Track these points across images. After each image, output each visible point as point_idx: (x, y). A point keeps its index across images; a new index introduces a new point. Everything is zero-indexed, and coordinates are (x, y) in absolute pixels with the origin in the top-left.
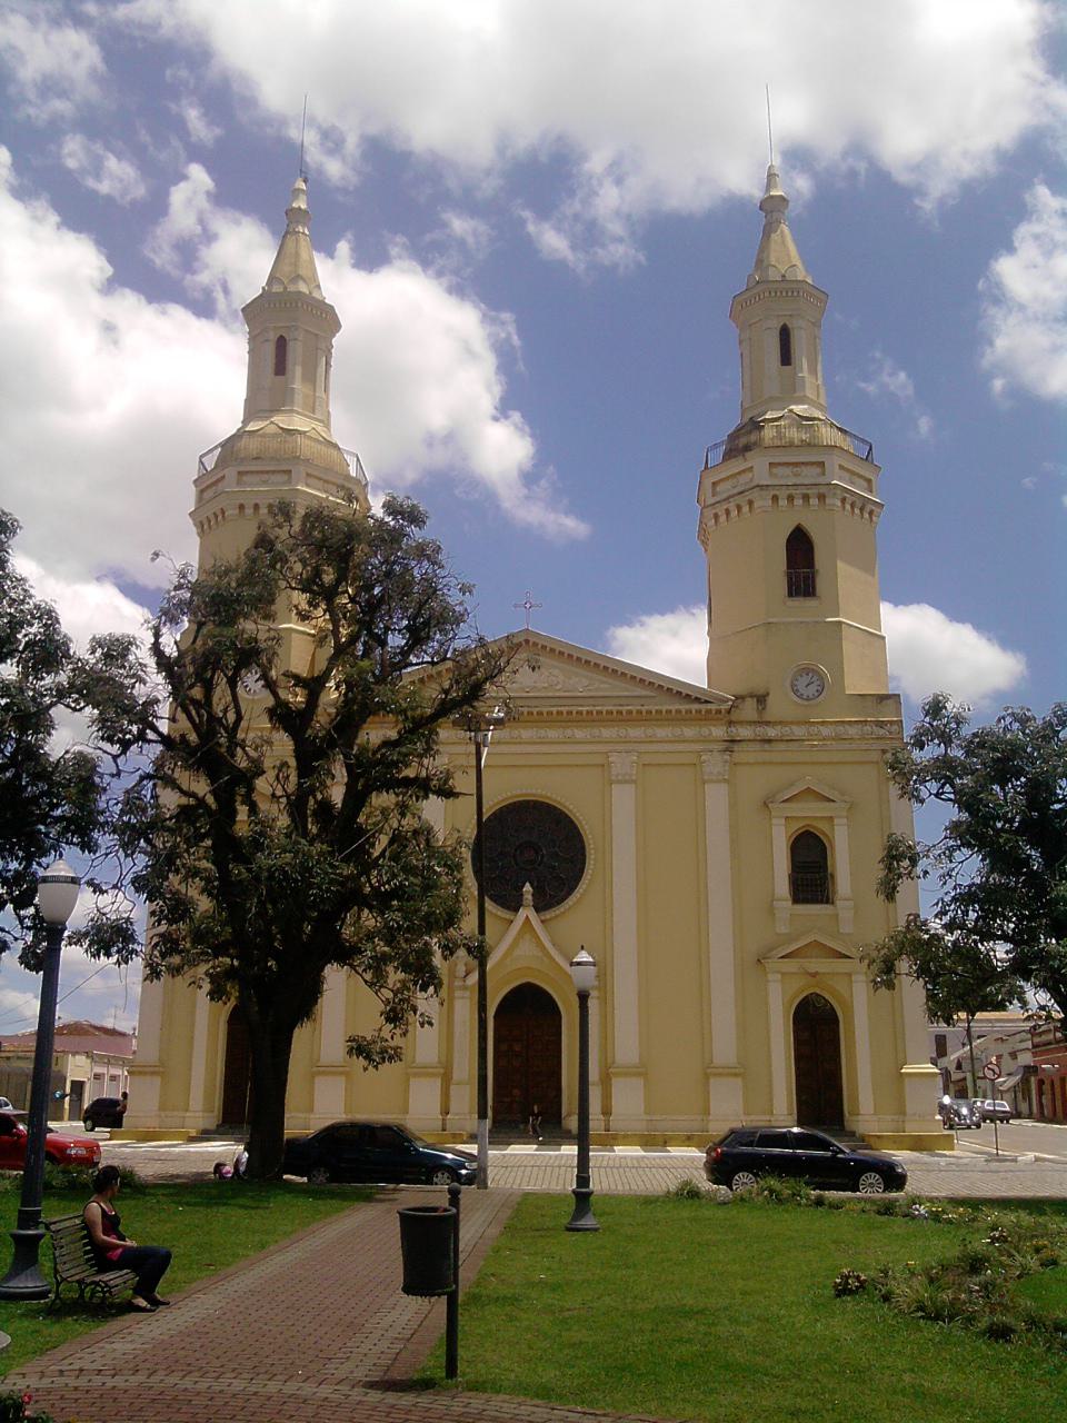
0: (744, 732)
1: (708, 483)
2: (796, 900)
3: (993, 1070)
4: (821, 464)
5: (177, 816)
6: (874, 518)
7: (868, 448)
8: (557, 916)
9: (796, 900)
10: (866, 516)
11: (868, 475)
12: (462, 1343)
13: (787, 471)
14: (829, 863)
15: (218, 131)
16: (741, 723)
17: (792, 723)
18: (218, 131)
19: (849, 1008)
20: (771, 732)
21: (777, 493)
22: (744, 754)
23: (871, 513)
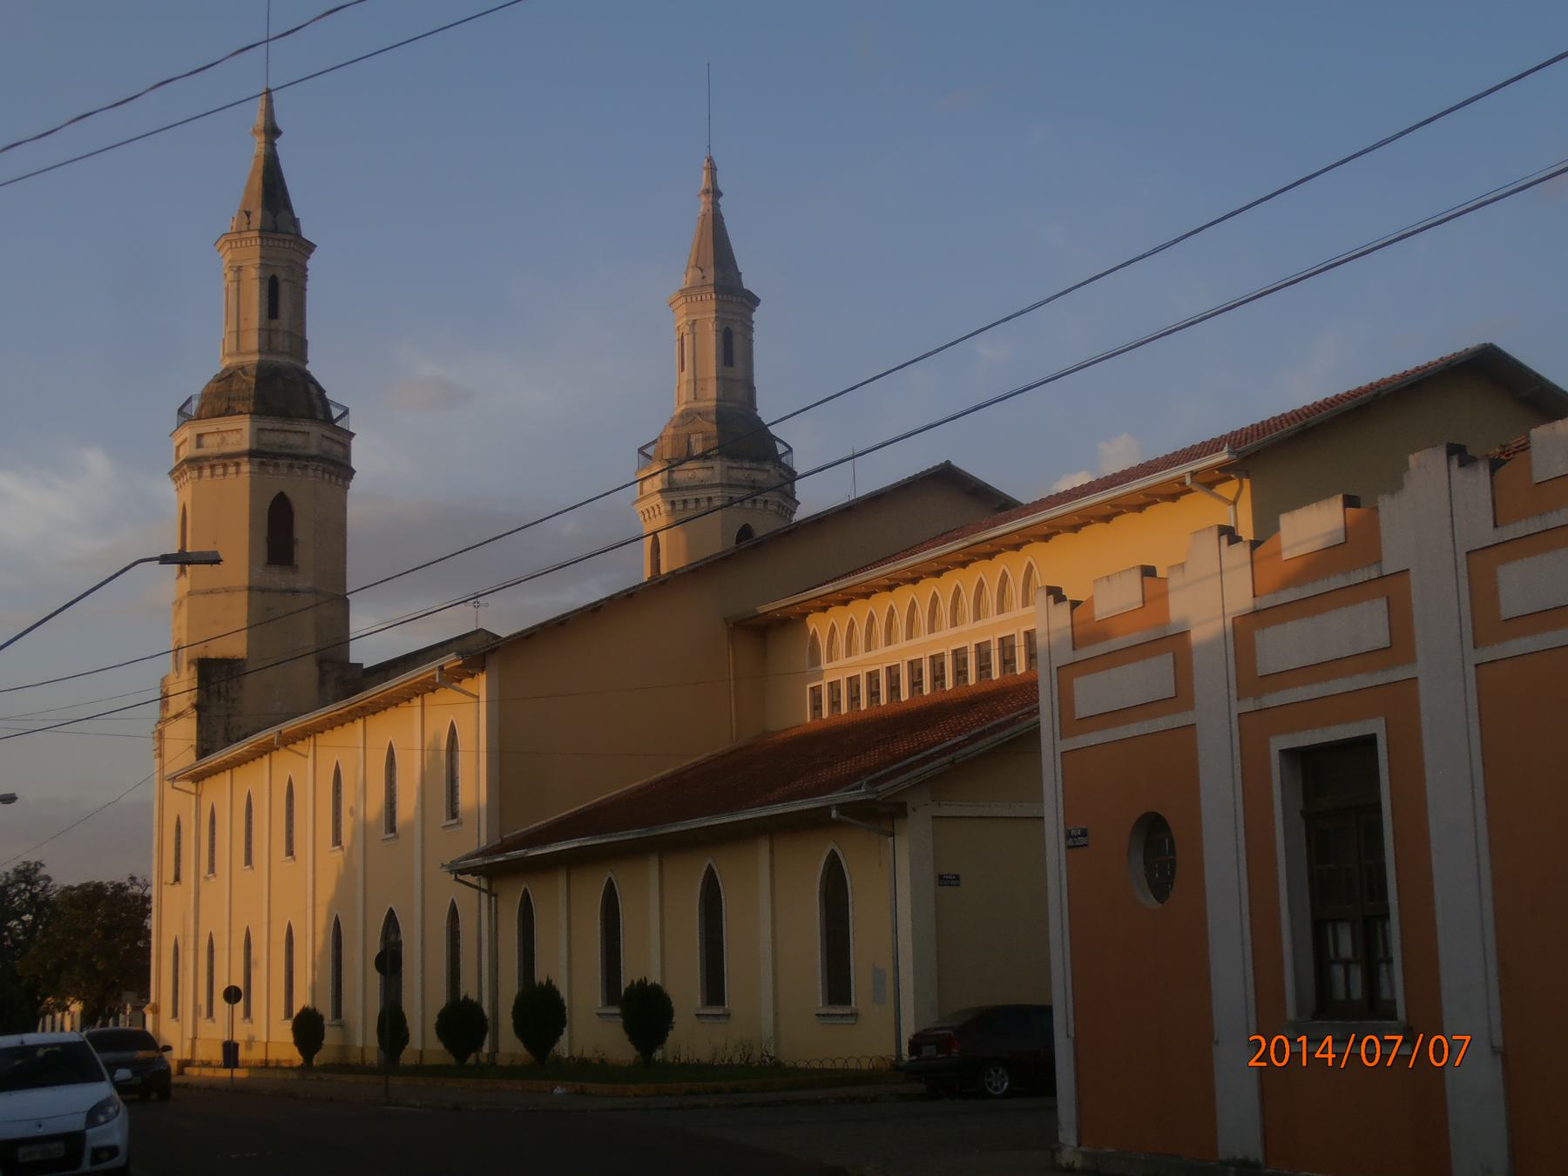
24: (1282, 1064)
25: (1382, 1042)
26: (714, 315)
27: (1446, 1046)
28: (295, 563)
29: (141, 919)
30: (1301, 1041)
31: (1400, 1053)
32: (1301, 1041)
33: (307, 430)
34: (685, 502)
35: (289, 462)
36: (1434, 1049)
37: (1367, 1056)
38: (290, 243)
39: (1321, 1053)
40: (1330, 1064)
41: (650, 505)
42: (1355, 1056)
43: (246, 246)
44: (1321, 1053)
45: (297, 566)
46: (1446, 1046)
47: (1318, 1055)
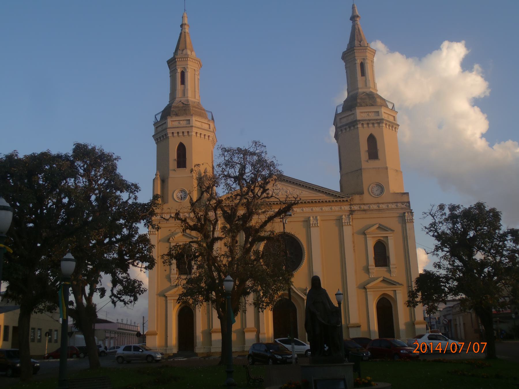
0: (356, 208)
1: (338, 118)
2: (376, 266)
3: (446, 321)
4: (378, 112)
5: (128, 279)
6: (396, 130)
7: (393, 105)
8: (289, 218)
9: (376, 266)
10: (394, 129)
11: (394, 115)
12: (260, 221)
13: (366, 114)
14: (393, 312)
15: (102, 274)
16: (355, 204)
17: (372, 204)
18: (102, 274)
19: (395, 302)
20: (366, 207)
21: (363, 122)
22: (356, 215)
23: (395, 128)
24: (477, 352)
25: (480, 345)
26: (177, 67)
27: (479, 346)
28: (379, 158)
29: (444, 291)
30: (431, 344)
31: (447, 349)
32: (431, 344)
33: (353, 113)
34: (178, 133)
35: (367, 122)
36: (475, 347)
37: (423, 350)
38: (364, 50)
39: (437, 348)
40: (440, 352)
41: (159, 137)
42: (471, 350)
43: (181, 60)
44: (437, 348)
45: (380, 159)
46: (479, 346)
47: (436, 349)
